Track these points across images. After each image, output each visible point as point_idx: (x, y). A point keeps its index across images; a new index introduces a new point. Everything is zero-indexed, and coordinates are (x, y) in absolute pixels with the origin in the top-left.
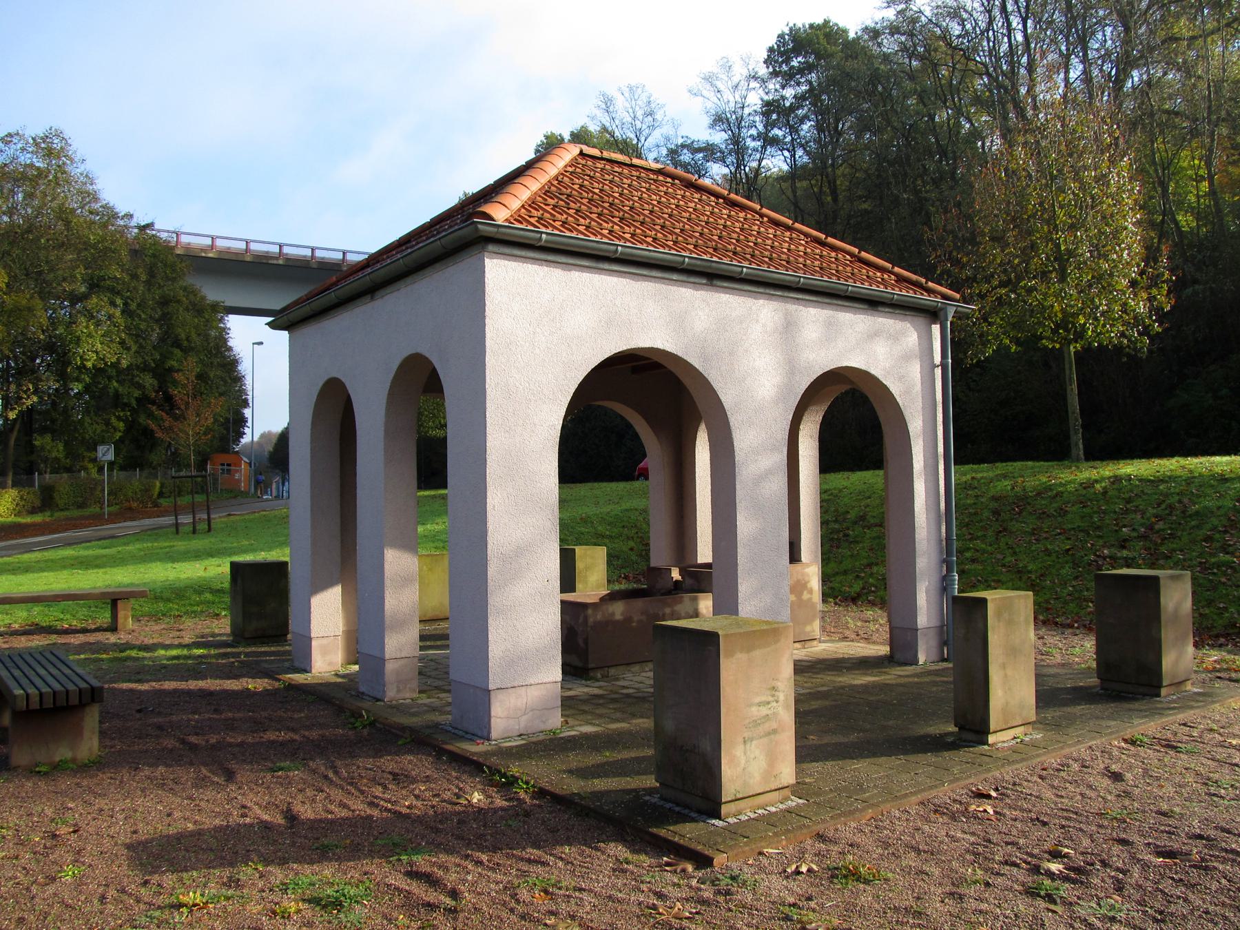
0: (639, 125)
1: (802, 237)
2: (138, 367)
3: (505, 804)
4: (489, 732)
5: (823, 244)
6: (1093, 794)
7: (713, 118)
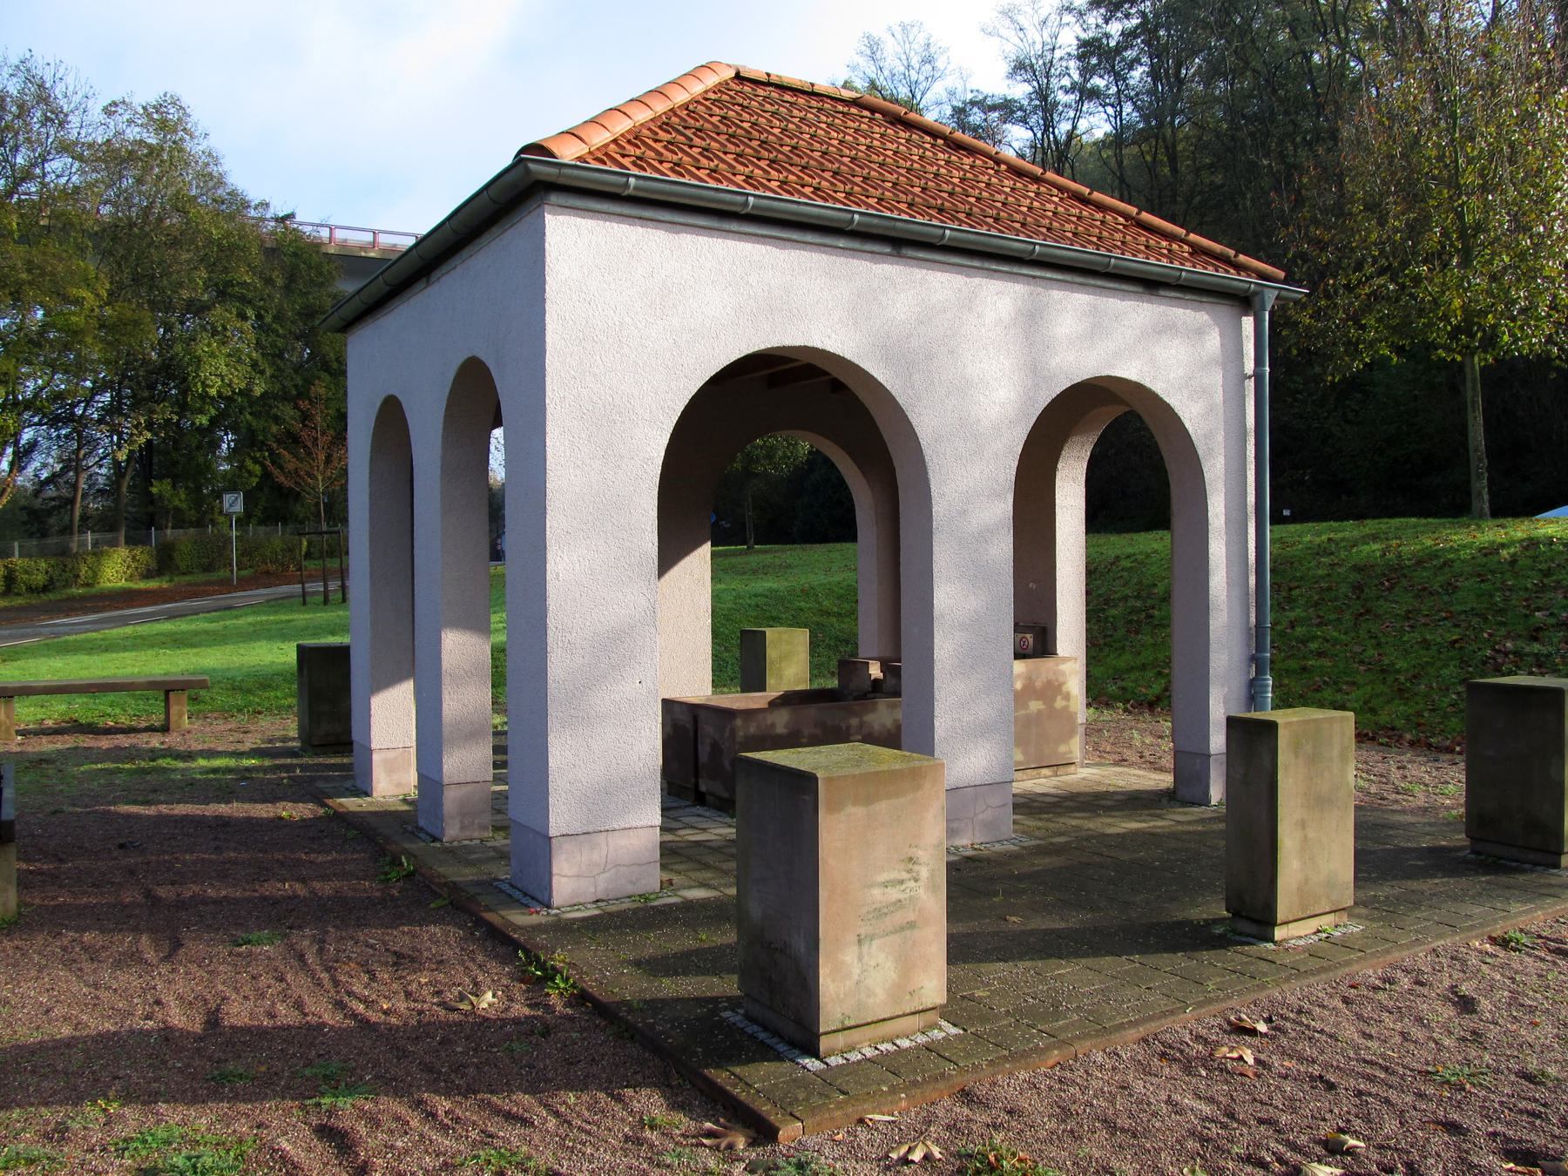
0: (914, 76)
1: (1055, 191)
2: (275, 397)
3: (526, 1011)
4: (550, 896)
5: (1084, 201)
6: (1418, 1033)
7: (1013, 64)
